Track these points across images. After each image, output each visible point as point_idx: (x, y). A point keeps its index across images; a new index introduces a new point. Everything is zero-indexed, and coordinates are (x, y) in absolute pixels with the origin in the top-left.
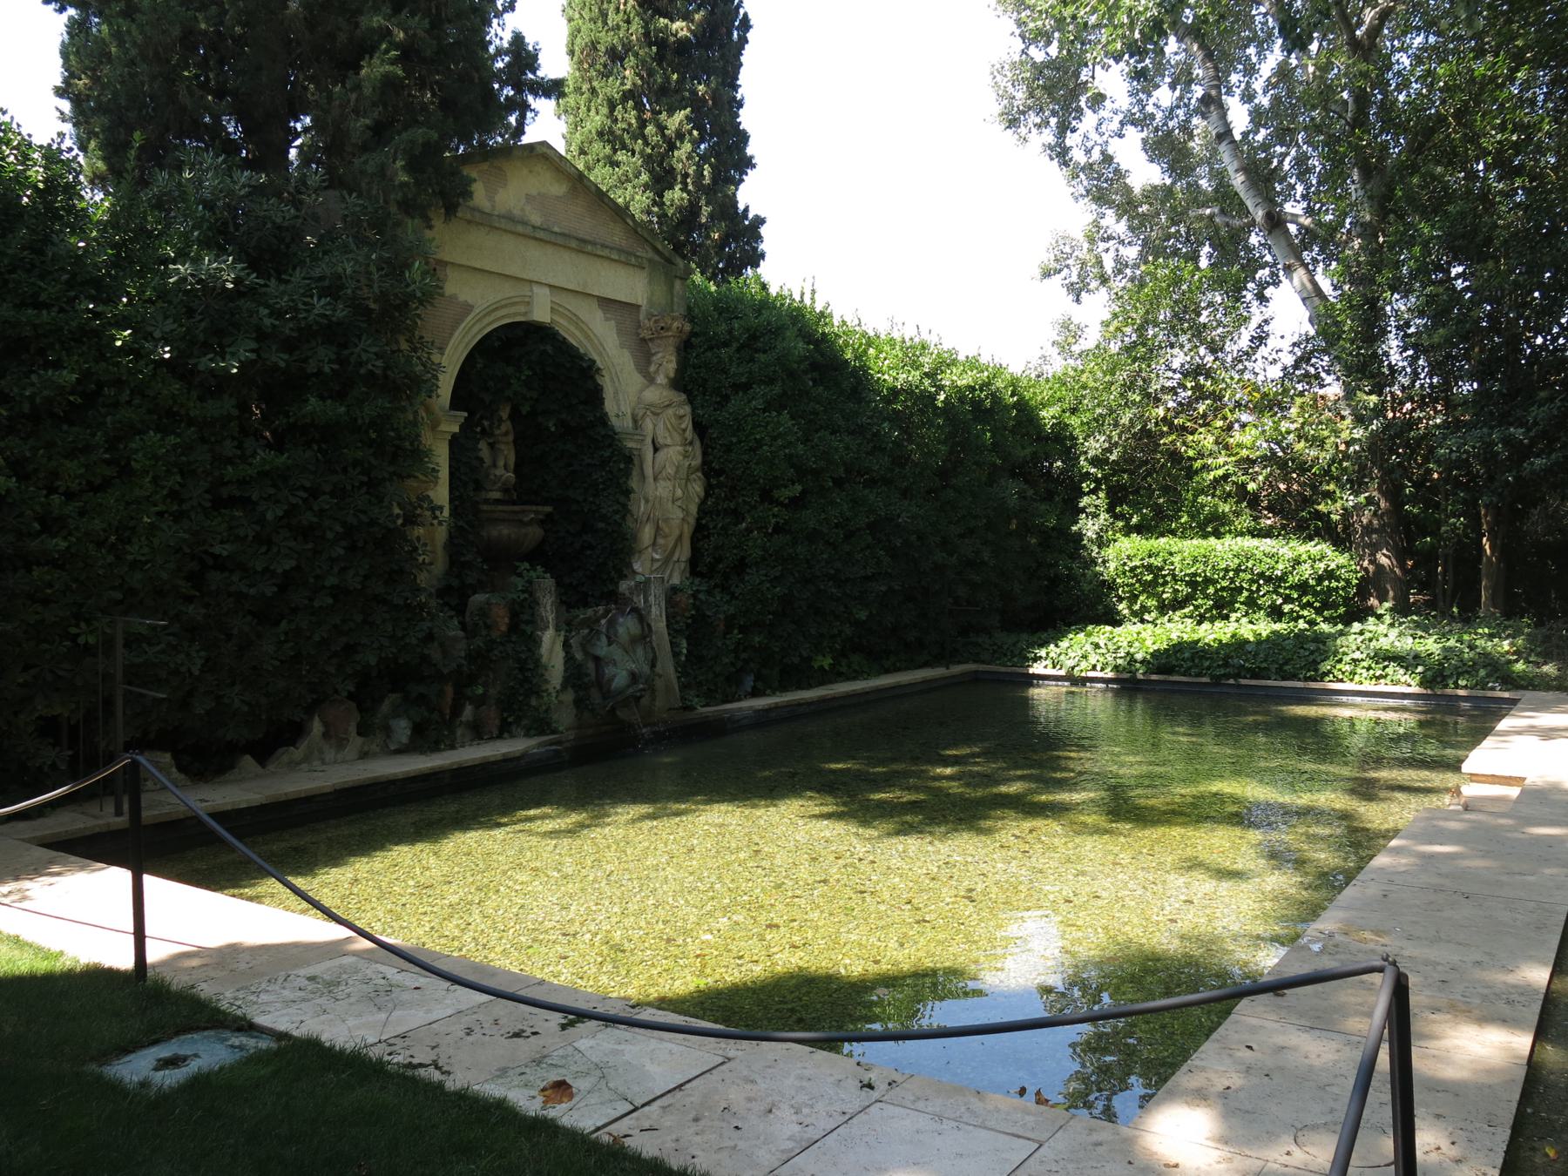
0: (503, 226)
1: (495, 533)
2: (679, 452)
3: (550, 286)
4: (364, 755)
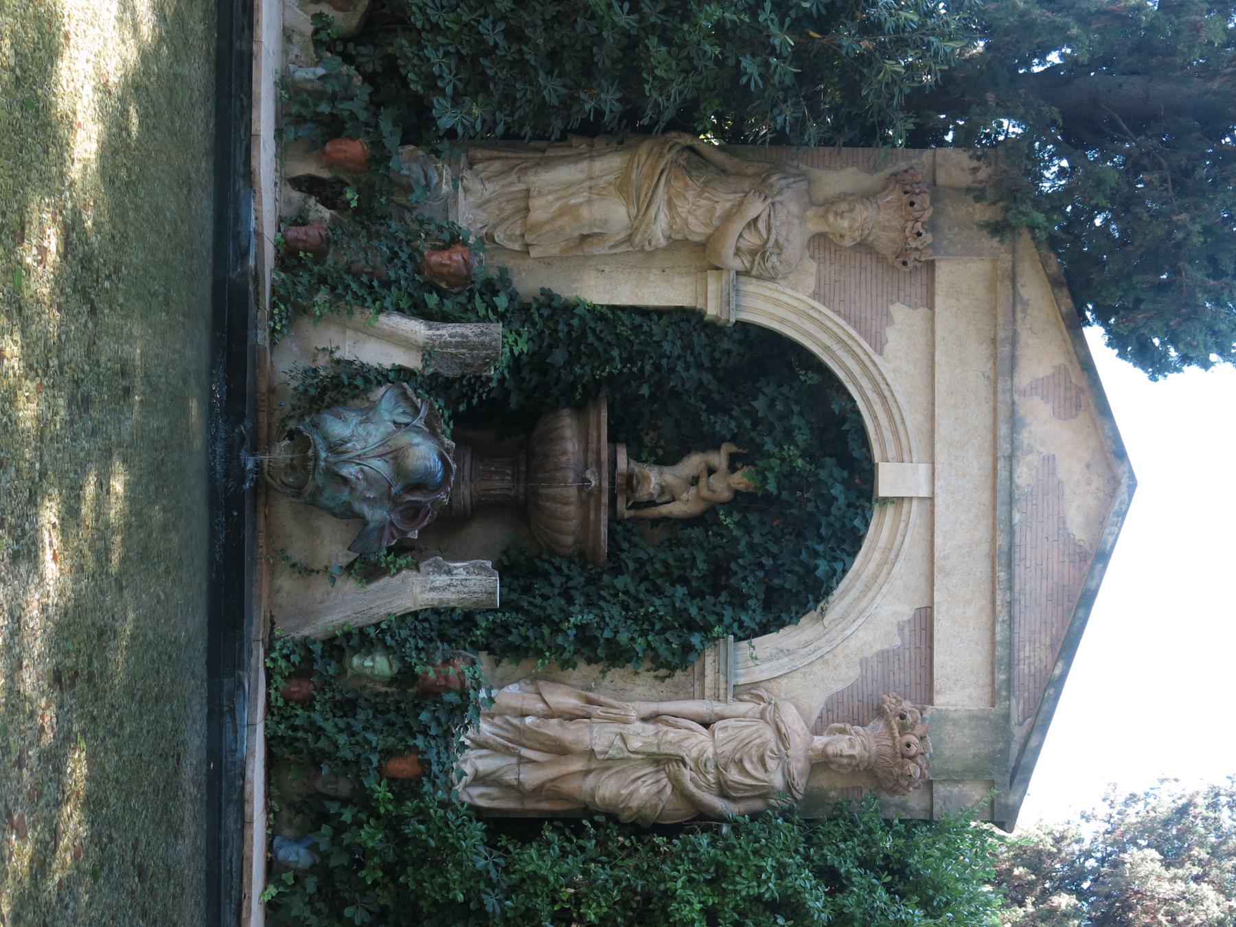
0: (1000, 397)
1: (568, 433)
2: (702, 752)
4: (287, 35)
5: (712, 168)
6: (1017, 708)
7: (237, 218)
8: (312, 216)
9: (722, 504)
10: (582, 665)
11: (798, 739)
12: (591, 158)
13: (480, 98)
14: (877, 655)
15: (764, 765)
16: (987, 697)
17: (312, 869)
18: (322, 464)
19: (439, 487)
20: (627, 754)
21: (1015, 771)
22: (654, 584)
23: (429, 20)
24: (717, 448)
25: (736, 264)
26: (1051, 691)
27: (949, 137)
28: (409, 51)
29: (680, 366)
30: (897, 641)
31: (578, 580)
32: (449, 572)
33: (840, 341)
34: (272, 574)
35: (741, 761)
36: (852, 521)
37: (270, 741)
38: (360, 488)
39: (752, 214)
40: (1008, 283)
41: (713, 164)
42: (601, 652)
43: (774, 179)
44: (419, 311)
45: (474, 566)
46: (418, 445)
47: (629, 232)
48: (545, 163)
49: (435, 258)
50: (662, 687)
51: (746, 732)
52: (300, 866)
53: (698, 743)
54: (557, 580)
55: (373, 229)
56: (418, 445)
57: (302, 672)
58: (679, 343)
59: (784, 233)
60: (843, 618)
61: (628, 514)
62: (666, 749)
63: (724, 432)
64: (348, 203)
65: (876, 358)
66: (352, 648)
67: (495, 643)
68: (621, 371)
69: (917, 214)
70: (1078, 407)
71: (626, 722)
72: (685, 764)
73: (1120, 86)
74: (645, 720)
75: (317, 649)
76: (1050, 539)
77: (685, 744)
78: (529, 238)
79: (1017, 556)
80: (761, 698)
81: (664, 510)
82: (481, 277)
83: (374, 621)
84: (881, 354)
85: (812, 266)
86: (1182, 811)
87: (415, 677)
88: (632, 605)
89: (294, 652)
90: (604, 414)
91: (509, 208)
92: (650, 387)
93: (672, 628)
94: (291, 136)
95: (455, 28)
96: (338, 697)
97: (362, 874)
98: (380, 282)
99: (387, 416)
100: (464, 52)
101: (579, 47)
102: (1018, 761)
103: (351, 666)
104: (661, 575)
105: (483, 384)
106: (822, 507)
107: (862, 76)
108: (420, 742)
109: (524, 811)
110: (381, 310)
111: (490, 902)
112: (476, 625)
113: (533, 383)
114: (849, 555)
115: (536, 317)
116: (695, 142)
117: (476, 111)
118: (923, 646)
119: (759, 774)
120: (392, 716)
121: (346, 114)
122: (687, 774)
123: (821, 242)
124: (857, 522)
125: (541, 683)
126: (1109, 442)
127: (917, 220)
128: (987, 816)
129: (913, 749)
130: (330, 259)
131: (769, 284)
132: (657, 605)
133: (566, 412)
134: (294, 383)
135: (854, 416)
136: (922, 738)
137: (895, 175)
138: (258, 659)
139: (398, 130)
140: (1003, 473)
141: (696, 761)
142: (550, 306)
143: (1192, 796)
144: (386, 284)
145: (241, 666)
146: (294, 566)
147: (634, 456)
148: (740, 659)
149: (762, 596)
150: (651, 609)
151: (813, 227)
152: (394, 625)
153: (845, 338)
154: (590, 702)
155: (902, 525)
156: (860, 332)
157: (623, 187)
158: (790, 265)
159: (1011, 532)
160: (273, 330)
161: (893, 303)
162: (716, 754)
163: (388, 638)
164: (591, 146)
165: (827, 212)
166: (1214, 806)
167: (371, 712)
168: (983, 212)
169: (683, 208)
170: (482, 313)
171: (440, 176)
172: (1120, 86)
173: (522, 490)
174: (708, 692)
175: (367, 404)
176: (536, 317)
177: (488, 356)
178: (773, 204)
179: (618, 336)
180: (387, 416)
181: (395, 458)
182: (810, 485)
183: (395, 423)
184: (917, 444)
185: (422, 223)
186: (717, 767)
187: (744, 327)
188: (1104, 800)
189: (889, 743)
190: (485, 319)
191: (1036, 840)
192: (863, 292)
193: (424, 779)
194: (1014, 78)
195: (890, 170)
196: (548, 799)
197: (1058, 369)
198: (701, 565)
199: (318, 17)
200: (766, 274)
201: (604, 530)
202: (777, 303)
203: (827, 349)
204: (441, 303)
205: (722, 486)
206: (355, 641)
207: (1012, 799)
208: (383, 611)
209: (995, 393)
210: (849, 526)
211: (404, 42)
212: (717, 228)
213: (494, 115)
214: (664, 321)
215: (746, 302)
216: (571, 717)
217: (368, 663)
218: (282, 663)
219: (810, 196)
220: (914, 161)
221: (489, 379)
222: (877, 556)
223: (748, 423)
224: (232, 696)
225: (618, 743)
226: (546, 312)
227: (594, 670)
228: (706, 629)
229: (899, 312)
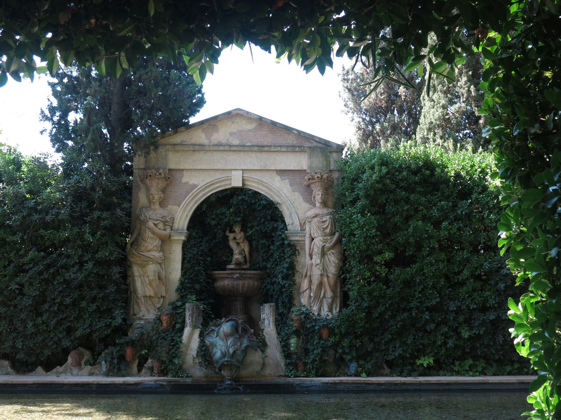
0: (211, 149)
1: (222, 284)
2: (321, 241)
3: (277, 171)
4: (91, 374)
5: (138, 238)
6: (307, 144)
7: (151, 388)
8: (150, 365)
9: (245, 234)
10: (295, 278)
11: (317, 211)
12: (134, 276)
13: (113, 311)
14: (291, 187)
15: (325, 221)
16: (304, 153)
17: (357, 362)
18: (229, 359)
19: (237, 322)
20: (321, 264)
21: (326, 145)
22: (269, 256)
23: (88, 327)
24: (228, 237)
25: (168, 230)
26: (302, 134)
27: (129, 163)
28: (98, 334)
29: (201, 248)
30: (287, 181)
31: (269, 280)
32: (264, 319)
33: (193, 198)
34: (265, 376)
35: (323, 228)
36: (250, 194)
37: (317, 376)
38: (237, 347)
39: (153, 225)
40: (176, 146)
41: (137, 237)
42: (291, 272)
43: (142, 219)
44: (182, 330)
45: (262, 311)
46: (223, 329)
47: (158, 264)
48: (135, 291)
49: (165, 325)
50: (302, 253)
51: (315, 227)
52: (356, 366)
53: (318, 242)
54: (269, 287)
55: (155, 345)
56: (223, 329)
57: (296, 366)
58: (194, 248)
59: (159, 215)
60: (280, 197)
61: (248, 265)
62: (320, 252)
63: (222, 234)
64: (146, 353)
65: (199, 187)
66: (288, 351)
67: (288, 306)
68: (203, 267)
69: (154, 174)
70: (215, 125)
71: (312, 264)
72: (324, 246)
73: (114, 111)
74: (311, 259)
75: (288, 361)
77: (318, 246)
78: (159, 296)
79: (260, 144)
80: (304, 222)
81: (247, 253)
82: (171, 311)
83: (279, 343)
84: (198, 185)
85: (170, 207)
86: (349, 90)
87: (297, 330)
88: (276, 263)
89: (289, 369)
90: (216, 272)
91: (149, 302)
92: (208, 257)
93: (283, 250)
94: (124, 372)
95: (91, 319)
96: (304, 354)
97: (358, 346)
98: (172, 342)
99: (214, 339)
100: (98, 316)
101: (98, 280)
102: (323, 144)
103: (294, 351)
104: (267, 254)
105: (205, 310)
106: (245, 203)
107: (108, 190)
108: (317, 328)
109: (340, 296)
110: (181, 342)
111: (365, 305)
112: (282, 312)
113: (206, 295)
114: (260, 195)
115: (184, 294)
116: (130, 243)
117: (117, 312)
119: (327, 223)
120: (309, 337)
121: (117, 354)
122: (328, 245)
123: (162, 204)
124: (250, 192)
125: (301, 291)
126: (225, 116)
127: (156, 174)
128: (340, 154)
129: (319, 176)
130: (164, 359)
131: (175, 220)
132: (276, 255)
133: (216, 284)
134: (204, 370)
135: (217, 194)
136: (316, 173)
137: (141, 181)
138: (291, 380)
139: (123, 337)
140: (235, 148)
141: (323, 242)
142: (181, 289)
143: (344, 87)
144: (173, 340)
145: (293, 384)
146: (262, 369)
147: (230, 263)
148: (293, 229)
149: (273, 222)
150: (277, 257)
151: (157, 206)
152: (281, 337)
153: (192, 196)
154: (306, 276)
155: (251, 179)
156: (191, 192)
157: (143, 266)
158: (169, 214)
159: (253, 146)
160: (187, 377)
161: (181, 182)
162: (321, 236)
163: (284, 339)
164: (130, 276)
165: (152, 202)
166: (347, 80)
167: (308, 344)
168: (153, 155)
169: (150, 247)
170: (182, 310)
171: (138, 324)
172: (114, 111)
173: (240, 298)
175: (211, 346)
176: (184, 294)
177: (196, 308)
178: (150, 219)
179: (191, 268)
180: (214, 339)
181: (227, 336)
182: (239, 207)
183: (216, 337)
184: (226, 174)
185: (153, 330)
186: (325, 236)
187: (189, 228)
188: (347, 114)
189: (318, 183)
190: (184, 309)
191: (359, 136)
192: (178, 191)
193: (329, 326)
194: (111, 144)
195: (140, 183)
196: (336, 289)
197: (203, 131)
198: (264, 241)
199: (86, 364)
200: (172, 221)
201: (253, 272)
202: (181, 218)
203: (196, 202)
204: (179, 323)
205: (240, 235)
206: (286, 349)
207: (335, 146)
208: (276, 340)
209: (210, 151)
210: (251, 195)
211: (95, 335)
212: (157, 236)
213: (118, 306)
214: (186, 253)
215: (181, 227)
216: (310, 282)
217: (293, 345)
218: (292, 372)
219: (148, 207)
220: (137, 175)
221: (204, 308)
222: (261, 187)
223: (219, 227)
224: (303, 387)
225: (318, 267)
226: (183, 290)
227: (297, 275)
228: (283, 239)
229: (184, 180)
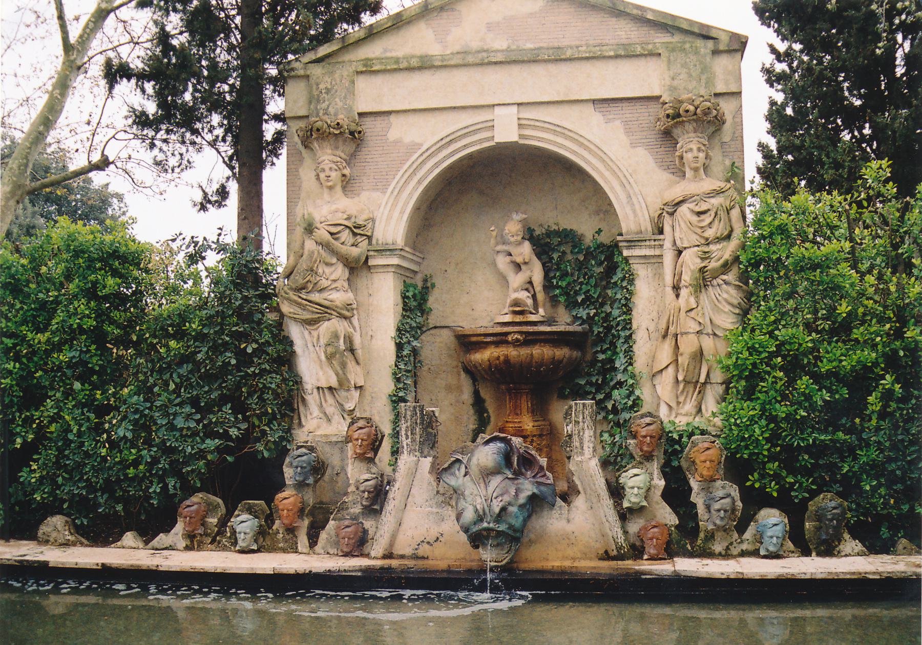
30: (618, 123)
32: (570, 436)
33: (414, 173)
74: (678, 296)
76: (544, 22)
84: (422, 145)
118: (621, 105)
141: (703, 259)
153: (411, 170)
174: (657, 252)
180: (460, 481)
183: (465, 475)
203: (419, 182)
229: (393, 135)
